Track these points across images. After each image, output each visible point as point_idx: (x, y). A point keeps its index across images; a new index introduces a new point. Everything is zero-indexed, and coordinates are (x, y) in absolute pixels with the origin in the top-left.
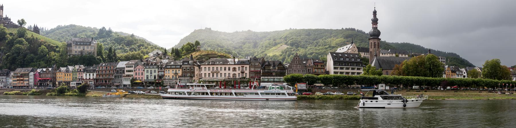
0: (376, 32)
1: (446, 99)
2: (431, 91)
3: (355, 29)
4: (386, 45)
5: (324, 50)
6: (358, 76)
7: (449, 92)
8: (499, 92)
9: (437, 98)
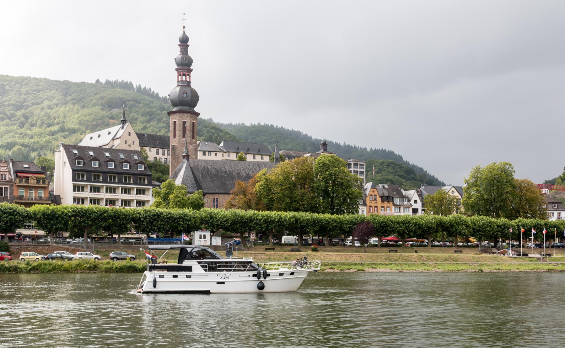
0: (186, 94)
1: (368, 269)
2: (329, 249)
3: (132, 85)
4: (213, 131)
5: (48, 138)
6: (139, 211)
7: (375, 252)
8: (510, 251)
9: (345, 267)
